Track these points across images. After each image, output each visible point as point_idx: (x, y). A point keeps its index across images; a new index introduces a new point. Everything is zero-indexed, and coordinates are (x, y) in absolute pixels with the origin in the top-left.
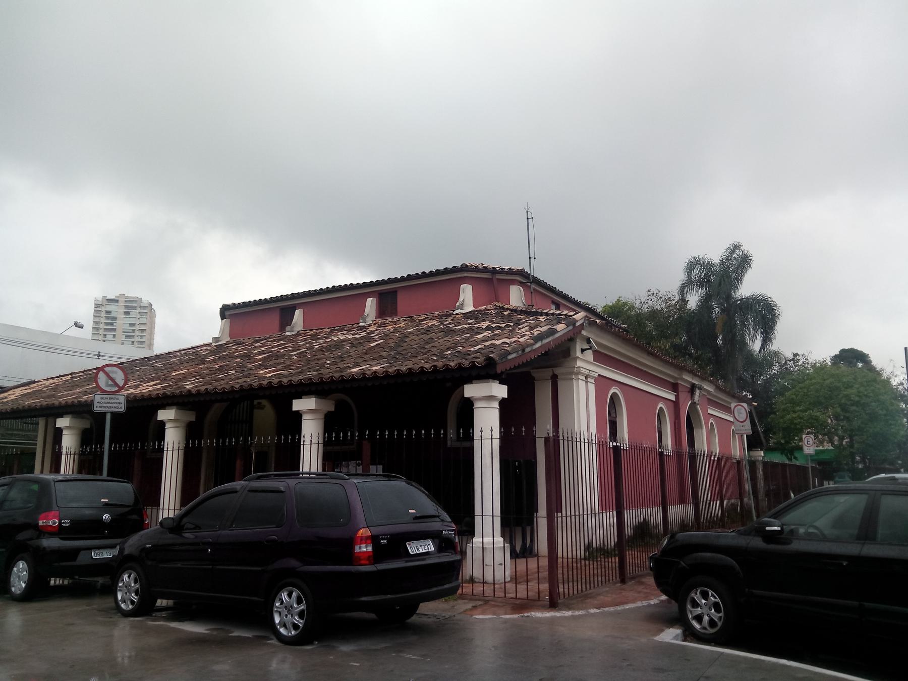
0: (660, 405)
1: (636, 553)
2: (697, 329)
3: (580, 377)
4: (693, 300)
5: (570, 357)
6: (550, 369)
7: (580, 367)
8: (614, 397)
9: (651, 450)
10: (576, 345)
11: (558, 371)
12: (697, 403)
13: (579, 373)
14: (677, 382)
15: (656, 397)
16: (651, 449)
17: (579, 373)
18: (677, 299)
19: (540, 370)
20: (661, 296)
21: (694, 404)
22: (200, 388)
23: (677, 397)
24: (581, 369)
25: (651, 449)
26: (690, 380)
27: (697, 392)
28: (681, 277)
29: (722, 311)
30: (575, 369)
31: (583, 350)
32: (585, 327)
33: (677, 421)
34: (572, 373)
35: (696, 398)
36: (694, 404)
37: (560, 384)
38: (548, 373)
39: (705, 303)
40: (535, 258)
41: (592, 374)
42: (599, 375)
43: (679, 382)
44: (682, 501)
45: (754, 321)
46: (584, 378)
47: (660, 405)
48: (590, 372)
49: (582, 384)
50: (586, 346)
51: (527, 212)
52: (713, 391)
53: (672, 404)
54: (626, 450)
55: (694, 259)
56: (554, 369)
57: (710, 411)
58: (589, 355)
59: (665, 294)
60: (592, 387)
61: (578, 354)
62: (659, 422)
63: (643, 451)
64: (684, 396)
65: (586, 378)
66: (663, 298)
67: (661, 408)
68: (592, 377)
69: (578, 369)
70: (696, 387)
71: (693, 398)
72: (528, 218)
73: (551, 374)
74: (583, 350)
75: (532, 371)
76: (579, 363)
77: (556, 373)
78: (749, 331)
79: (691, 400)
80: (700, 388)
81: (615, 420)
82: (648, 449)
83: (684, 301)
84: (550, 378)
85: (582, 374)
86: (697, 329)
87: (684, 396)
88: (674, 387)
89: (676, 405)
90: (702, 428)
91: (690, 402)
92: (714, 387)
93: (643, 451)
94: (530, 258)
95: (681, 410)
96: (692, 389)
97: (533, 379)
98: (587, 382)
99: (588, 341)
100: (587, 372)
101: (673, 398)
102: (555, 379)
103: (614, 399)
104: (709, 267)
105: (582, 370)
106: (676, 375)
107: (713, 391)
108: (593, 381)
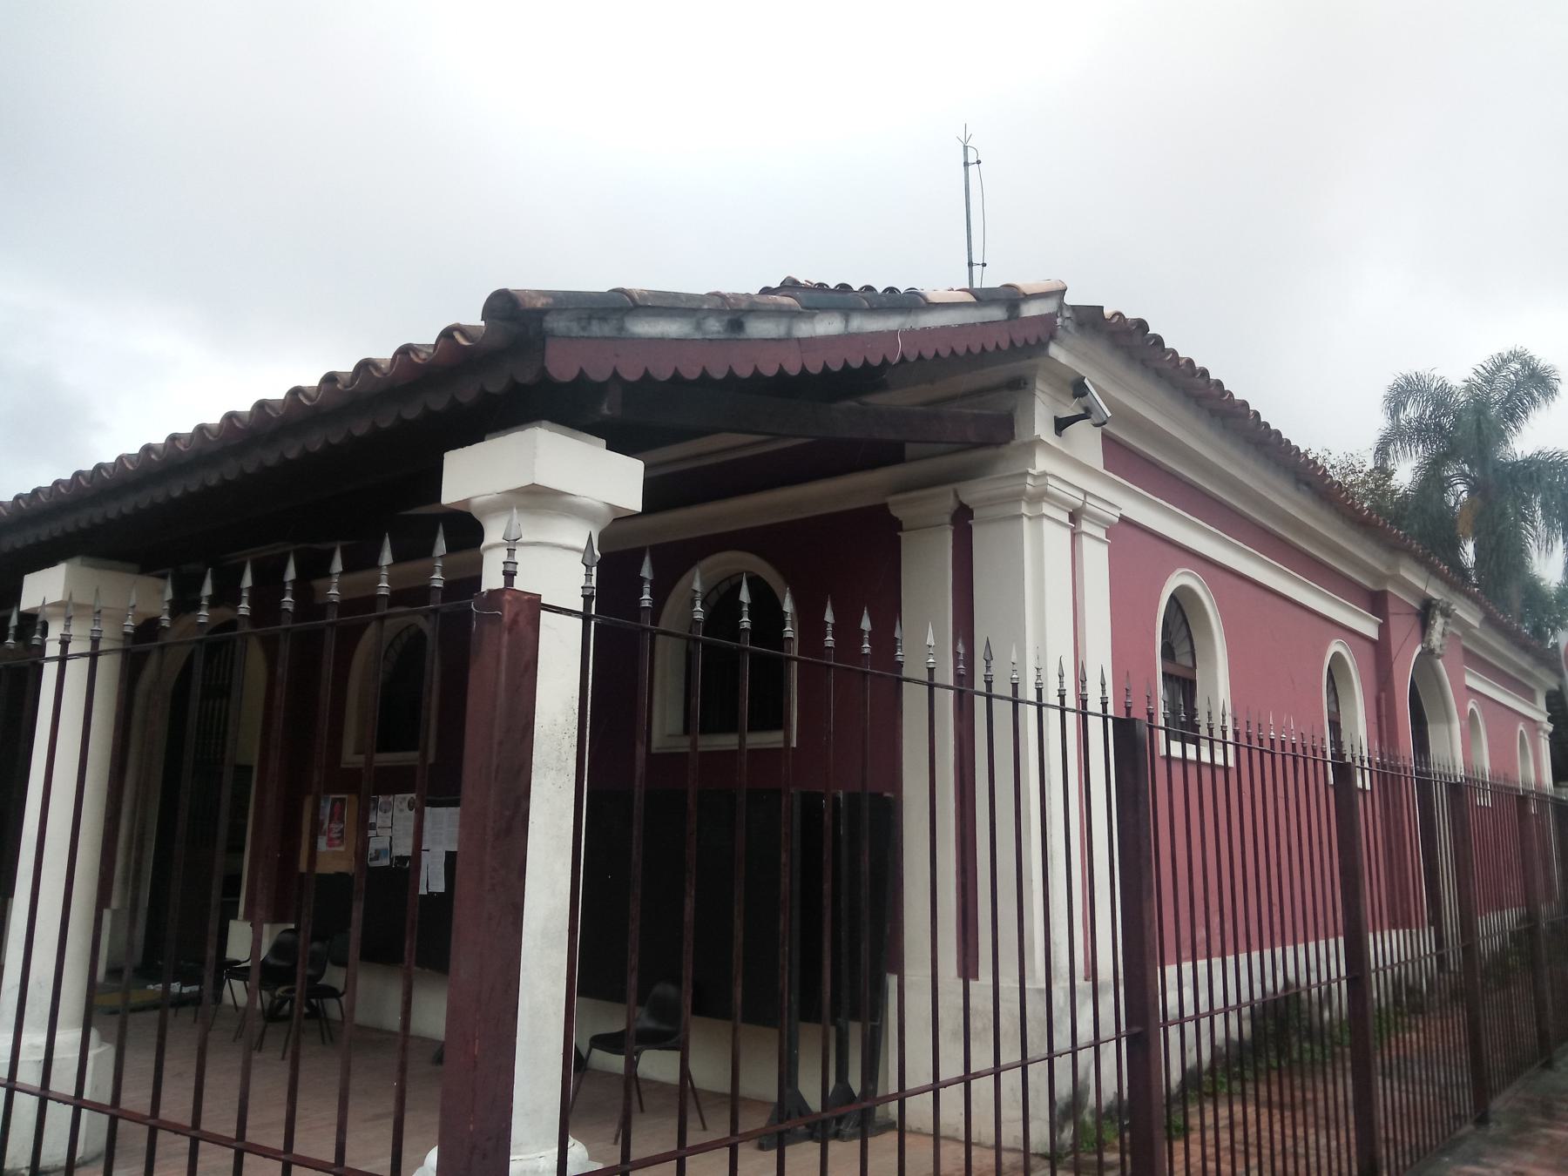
0: (1335, 647)
1: (1251, 1110)
2: (1416, 527)
3: (1047, 509)
4: (1405, 473)
5: (1013, 443)
6: (949, 488)
7: (1044, 474)
8: (1181, 605)
9: (1300, 757)
10: (1033, 404)
11: (973, 493)
12: (1438, 651)
13: (1042, 496)
14: (1381, 589)
15: (1322, 624)
16: (1299, 751)
17: (1042, 496)
18: (1370, 465)
19: (914, 494)
20: (1333, 462)
21: (1428, 654)
22: (250, 631)
23: (1384, 629)
24: (1051, 481)
25: (1299, 751)
26: (1421, 585)
27: (1439, 623)
28: (1380, 423)
29: (1471, 492)
30: (1029, 480)
31: (1061, 425)
32: (1060, 333)
33: (1383, 695)
34: (1017, 497)
35: (1436, 638)
36: (1428, 654)
37: (983, 539)
38: (943, 502)
39: (1432, 479)
40: (984, 265)
41: (1093, 506)
42: (1123, 519)
43: (1389, 589)
44: (1400, 919)
45: (1544, 506)
46: (1065, 518)
47: (1335, 647)
48: (1089, 500)
49: (1056, 538)
50: (1070, 409)
51: (966, 148)
52: (1476, 624)
53: (1368, 649)
54: (1226, 767)
55: (1406, 378)
56: (956, 486)
57: (1471, 681)
58: (1086, 442)
59: (1343, 458)
60: (1096, 556)
61: (1042, 428)
62: (1332, 697)
63: (1267, 757)
64: (1402, 628)
65: (1075, 516)
66: (1338, 468)
67: (1337, 657)
68: (1097, 519)
69: (1039, 482)
70: (1435, 606)
71: (1426, 639)
72: (966, 164)
73: (950, 504)
74: (1061, 425)
75: (890, 500)
76: (1042, 463)
77: (965, 499)
78: (1533, 527)
79: (1423, 642)
80: (1446, 614)
81: (1187, 675)
82: (1289, 749)
83: (1383, 472)
84: (947, 519)
85: (1059, 502)
86: (1416, 527)
87: (1402, 628)
88: (1376, 603)
89: (1380, 653)
90: (1449, 720)
91: (1418, 649)
92: (1481, 616)
93: (1267, 757)
94: (970, 264)
95: (1394, 666)
96: (1425, 612)
97: (897, 525)
98: (1075, 535)
99: (1079, 389)
100: (1076, 499)
101: (1369, 628)
102: (963, 519)
103: (1182, 609)
104: (1440, 398)
105: (1054, 486)
106: (1382, 569)
107: (1476, 624)
108: (1101, 534)
